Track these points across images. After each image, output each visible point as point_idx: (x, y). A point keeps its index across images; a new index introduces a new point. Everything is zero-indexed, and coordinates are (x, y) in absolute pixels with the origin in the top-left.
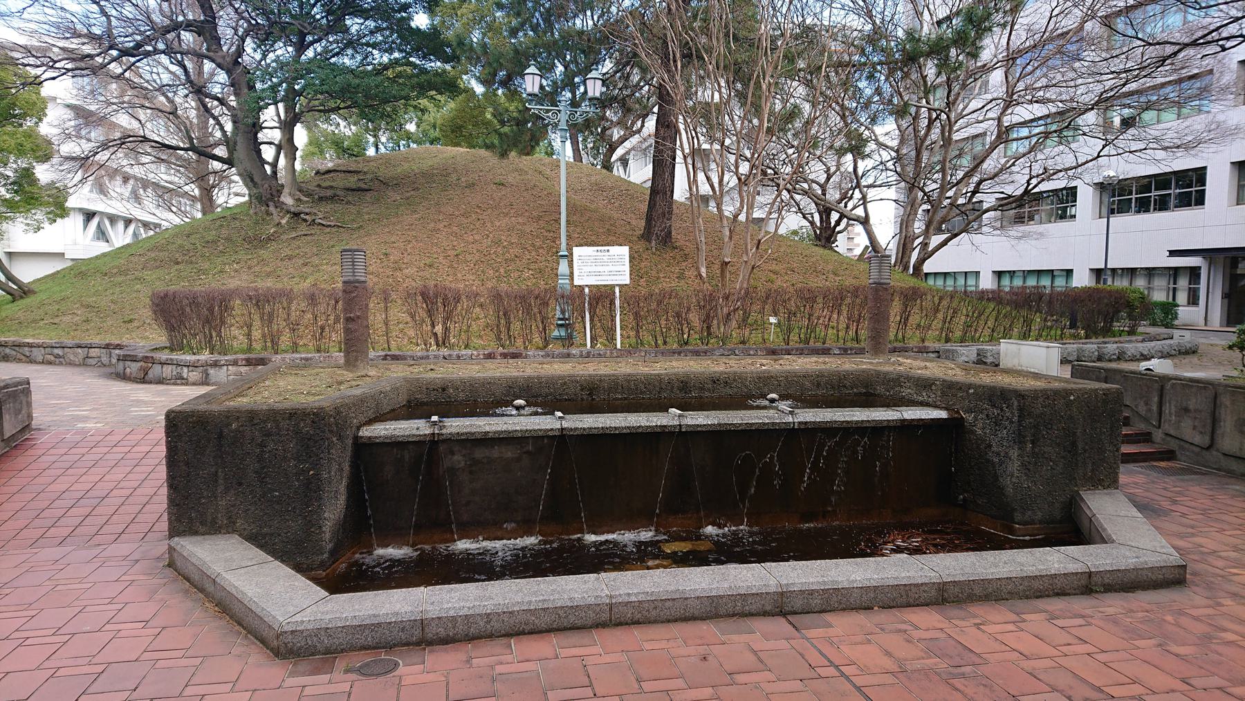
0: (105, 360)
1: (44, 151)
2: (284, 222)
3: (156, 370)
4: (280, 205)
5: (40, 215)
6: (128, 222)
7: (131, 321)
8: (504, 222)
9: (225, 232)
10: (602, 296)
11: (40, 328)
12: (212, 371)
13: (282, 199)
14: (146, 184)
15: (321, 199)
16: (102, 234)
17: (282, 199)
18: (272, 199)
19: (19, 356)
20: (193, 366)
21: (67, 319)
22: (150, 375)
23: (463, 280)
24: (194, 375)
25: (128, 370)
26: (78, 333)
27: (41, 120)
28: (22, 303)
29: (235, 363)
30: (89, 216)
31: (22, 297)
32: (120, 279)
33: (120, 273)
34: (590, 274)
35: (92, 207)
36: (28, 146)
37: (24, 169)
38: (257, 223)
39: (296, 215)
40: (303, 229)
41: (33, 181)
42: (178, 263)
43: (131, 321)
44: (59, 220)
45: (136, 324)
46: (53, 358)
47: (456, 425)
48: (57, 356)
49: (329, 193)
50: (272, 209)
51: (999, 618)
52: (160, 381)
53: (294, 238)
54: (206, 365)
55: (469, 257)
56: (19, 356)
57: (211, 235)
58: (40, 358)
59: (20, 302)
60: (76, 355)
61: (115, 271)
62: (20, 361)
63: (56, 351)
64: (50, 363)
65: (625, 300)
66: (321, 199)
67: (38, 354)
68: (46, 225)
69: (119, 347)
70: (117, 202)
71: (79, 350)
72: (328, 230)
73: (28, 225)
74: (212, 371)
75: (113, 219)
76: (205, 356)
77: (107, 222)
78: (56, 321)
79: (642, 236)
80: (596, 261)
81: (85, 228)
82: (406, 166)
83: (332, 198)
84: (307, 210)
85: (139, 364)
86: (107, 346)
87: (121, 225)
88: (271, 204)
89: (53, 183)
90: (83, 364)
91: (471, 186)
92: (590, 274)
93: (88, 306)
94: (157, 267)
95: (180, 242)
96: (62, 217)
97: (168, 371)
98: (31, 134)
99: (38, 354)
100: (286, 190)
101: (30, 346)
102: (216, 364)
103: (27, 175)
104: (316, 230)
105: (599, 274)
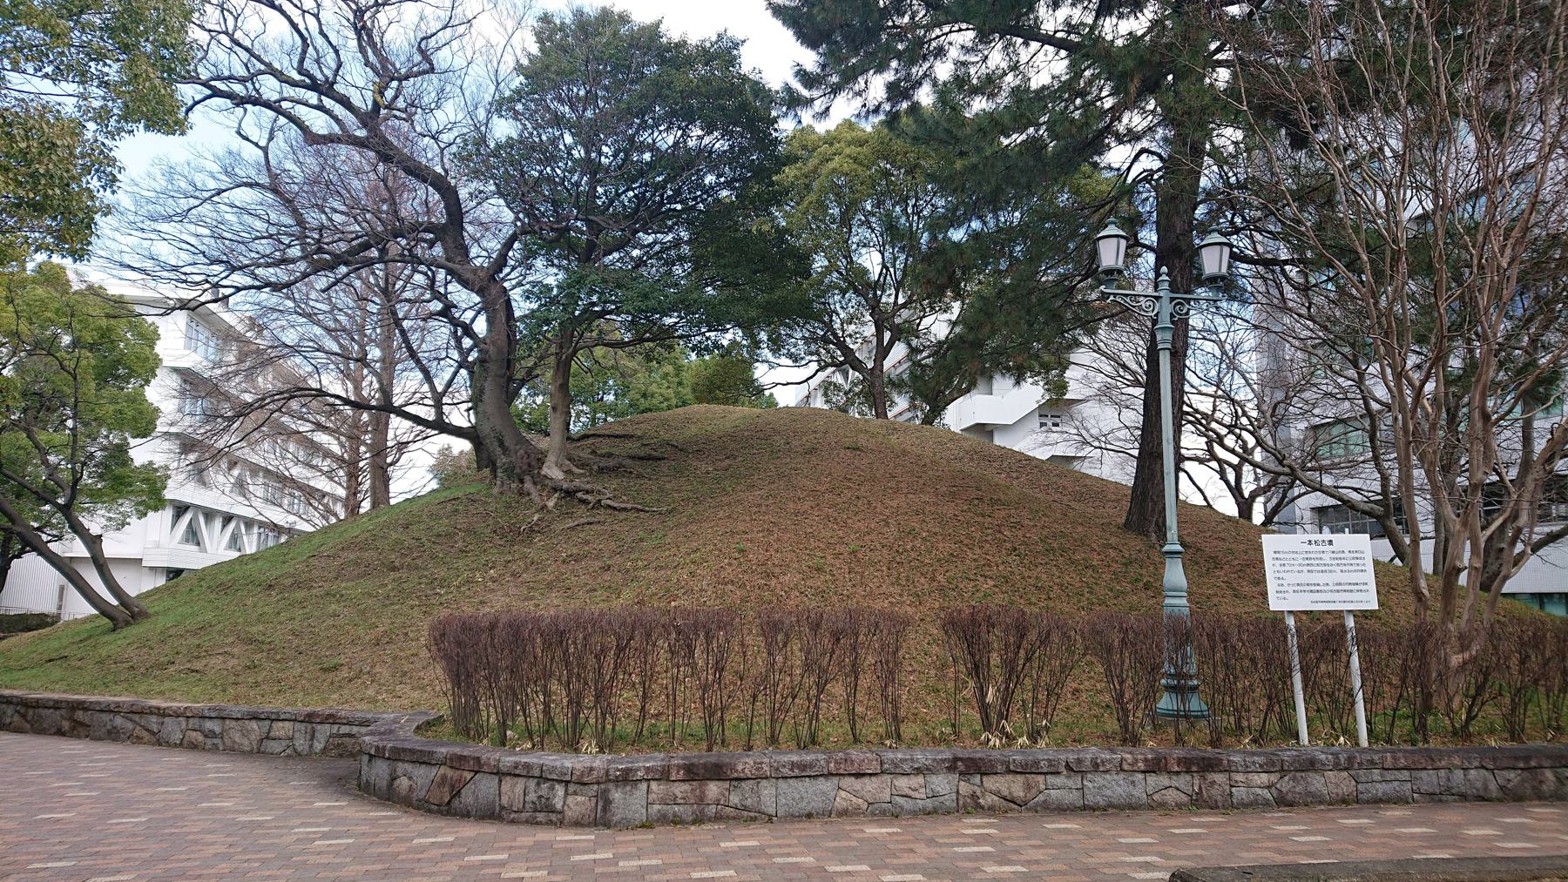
0: (301, 743)
1: (143, 422)
2: (551, 504)
3: (484, 788)
4: (541, 481)
5: (127, 507)
6: (228, 518)
7: (335, 668)
8: (900, 500)
9: (462, 521)
10: (1323, 633)
11: (170, 678)
12: (616, 795)
13: (545, 471)
14: (255, 470)
15: (601, 470)
16: (193, 536)
17: (545, 471)
18: (529, 472)
19: (138, 731)
20: (571, 782)
21: (216, 661)
22: (467, 797)
23: (880, 594)
24: (579, 804)
25: (403, 783)
26: (241, 689)
27: (147, 382)
28: (134, 631)
29: (664, 775)
30: (181, 509)
31: (127, 624)
32: (300, 594)
33: (297, 585)
34: (1300, 588)
35: (187, 499)
36: (130, 413)
37: (117, 445)
38: (508, 506)
39: (569, 493)
40: (582, 515)
41: (126, 461)
42: (394, 569)
43: (335, 668)
44: (151, 514)
45: (344, 673)
46: (201, 738)
47: (790, 860)
48: (211, 734)
49: (612, 463)
50: (528, 485)
51: (103, 753)
52: (492, 814)
53: (572, 529)
54: (607, 779)
55: (876, 556)
56: (138, 731)
57: (443, 525)
58: (176, 737)
59: (125, 632)
60: (245, 733)
61: (288, 581)
62: (139, 740)
63: (209, 725)
64: (193, 747)
65: (1363, 638)
66: (601, 470)
67: (174, 730)
68: (133, 520)
69: (331, 719)
70: (217, 494)
71: (254, 725)
72: (622, 516)
73: (110, 519)
74: (616, 795)
75: (209, 514)
76: (589, 759)
77: (202, 519)
78: (198, 665)
79: (1127, 525)
80: (1309, 563)
81: (173, 526)
82: (694, 430)
83: (613, 471)
84: (588, 487)
85: (434, 772)
86: (310, 718)
87: (218, 523)
88: (527, 478)
89: (151, 463)
90: (258, 752)
91: (812, 451)
92: (1300, 588)
93: (251, 641)
94: (359, 576)
95: (394, 536)
96: (156, 509)
97: (513, 791)
98: (138, 399)
99: (174, 730)
100: (551, 458)
101: (162, 713)
102: (626, 779)
103: (119, 453)
104: (601, 515)
105: (1314, 589)
